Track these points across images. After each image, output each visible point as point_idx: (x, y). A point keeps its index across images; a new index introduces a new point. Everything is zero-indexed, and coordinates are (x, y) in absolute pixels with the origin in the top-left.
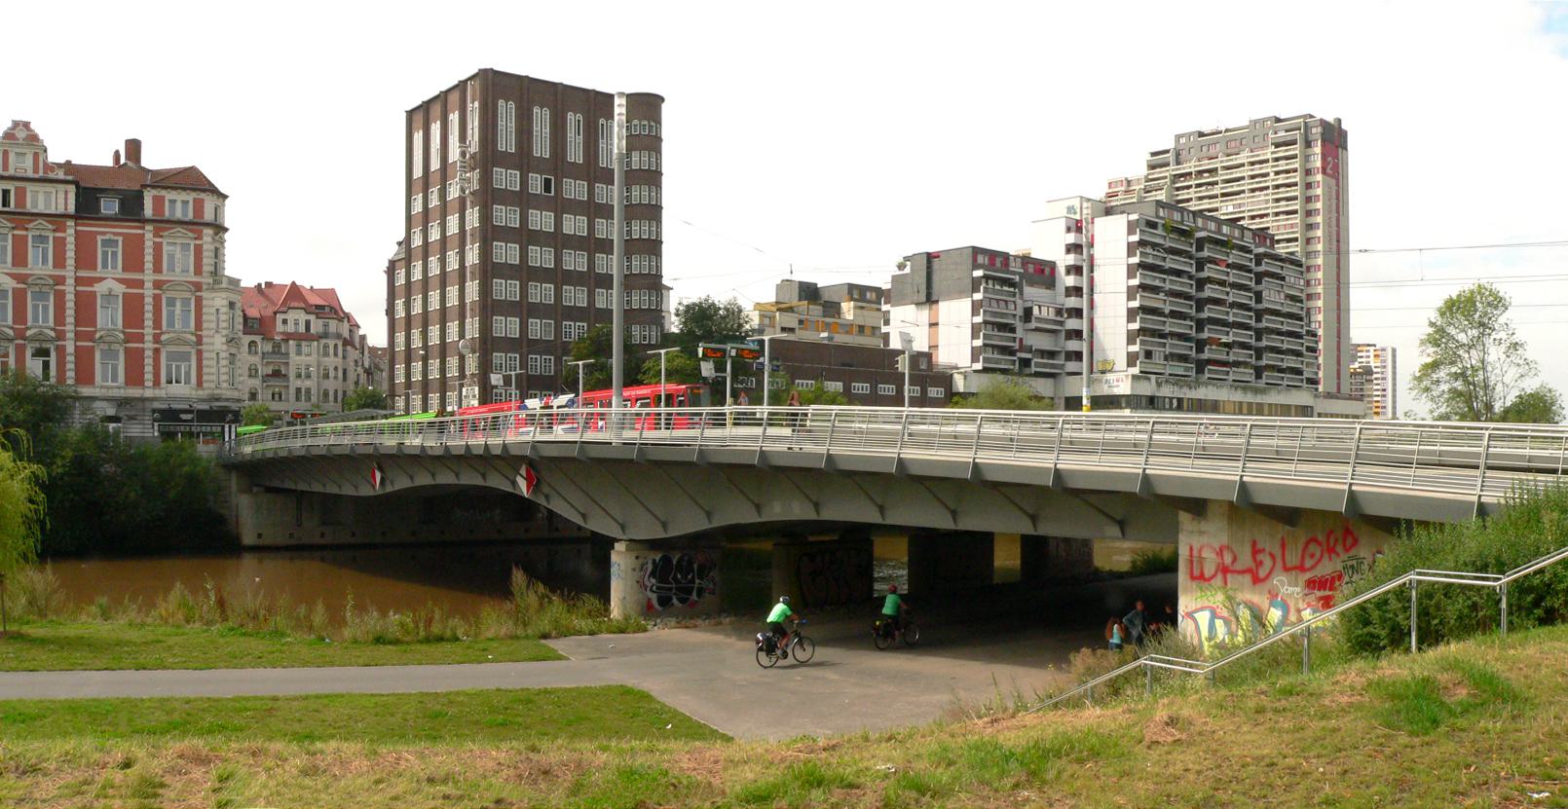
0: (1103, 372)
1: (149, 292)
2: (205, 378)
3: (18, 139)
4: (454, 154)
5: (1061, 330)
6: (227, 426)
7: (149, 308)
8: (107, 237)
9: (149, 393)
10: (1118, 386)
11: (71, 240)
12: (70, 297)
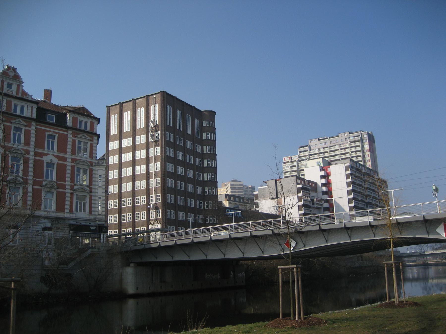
1: (69, 164)
3: (10, 76)
6: (102, 234)
7: (69, 171)
9: (67, 215)
11: (33, 132)
12: (31, 161)
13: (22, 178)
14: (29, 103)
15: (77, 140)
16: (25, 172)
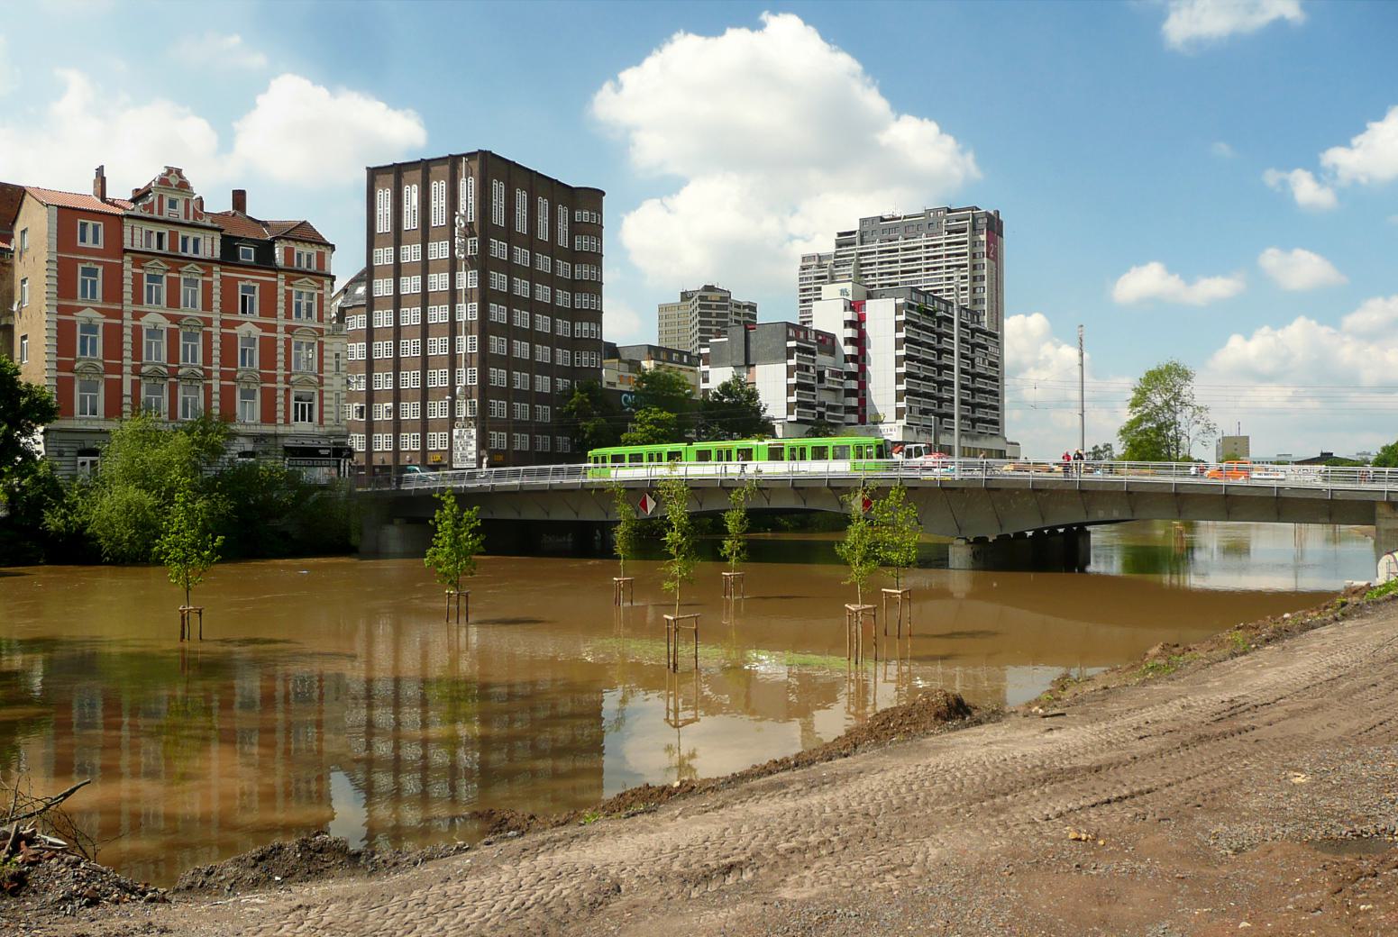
0: (875, 423)
1: (281, 336)
2: (325, 416)
3: (172, 185)
4: (438, 218)
5: (840, 390)
6: (343, 460)
7: (281, 350)
8: (87, 265)
9: (281, 430)
10: (891, 434)
11: (217, 284)
12: (216, 338)
13: (202, 369)
14: (207, 232)
15: (294, 290)
16: (208, 359)
